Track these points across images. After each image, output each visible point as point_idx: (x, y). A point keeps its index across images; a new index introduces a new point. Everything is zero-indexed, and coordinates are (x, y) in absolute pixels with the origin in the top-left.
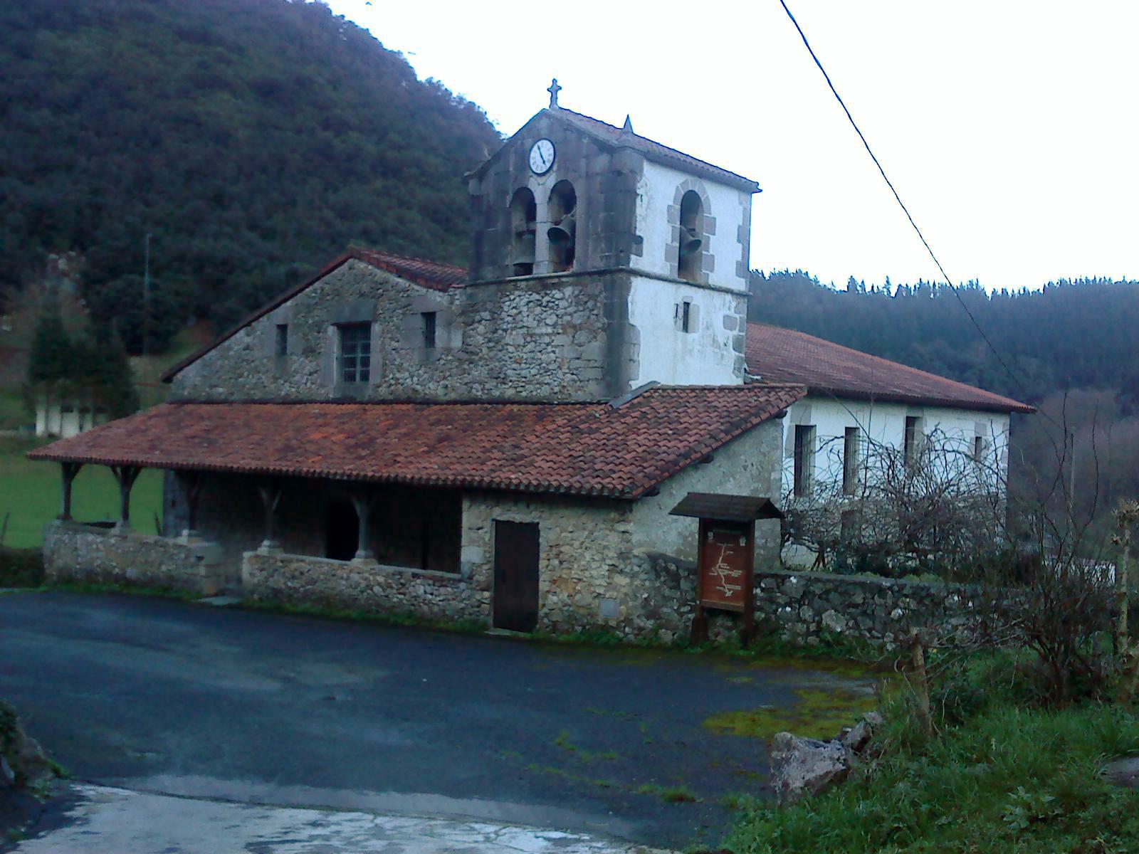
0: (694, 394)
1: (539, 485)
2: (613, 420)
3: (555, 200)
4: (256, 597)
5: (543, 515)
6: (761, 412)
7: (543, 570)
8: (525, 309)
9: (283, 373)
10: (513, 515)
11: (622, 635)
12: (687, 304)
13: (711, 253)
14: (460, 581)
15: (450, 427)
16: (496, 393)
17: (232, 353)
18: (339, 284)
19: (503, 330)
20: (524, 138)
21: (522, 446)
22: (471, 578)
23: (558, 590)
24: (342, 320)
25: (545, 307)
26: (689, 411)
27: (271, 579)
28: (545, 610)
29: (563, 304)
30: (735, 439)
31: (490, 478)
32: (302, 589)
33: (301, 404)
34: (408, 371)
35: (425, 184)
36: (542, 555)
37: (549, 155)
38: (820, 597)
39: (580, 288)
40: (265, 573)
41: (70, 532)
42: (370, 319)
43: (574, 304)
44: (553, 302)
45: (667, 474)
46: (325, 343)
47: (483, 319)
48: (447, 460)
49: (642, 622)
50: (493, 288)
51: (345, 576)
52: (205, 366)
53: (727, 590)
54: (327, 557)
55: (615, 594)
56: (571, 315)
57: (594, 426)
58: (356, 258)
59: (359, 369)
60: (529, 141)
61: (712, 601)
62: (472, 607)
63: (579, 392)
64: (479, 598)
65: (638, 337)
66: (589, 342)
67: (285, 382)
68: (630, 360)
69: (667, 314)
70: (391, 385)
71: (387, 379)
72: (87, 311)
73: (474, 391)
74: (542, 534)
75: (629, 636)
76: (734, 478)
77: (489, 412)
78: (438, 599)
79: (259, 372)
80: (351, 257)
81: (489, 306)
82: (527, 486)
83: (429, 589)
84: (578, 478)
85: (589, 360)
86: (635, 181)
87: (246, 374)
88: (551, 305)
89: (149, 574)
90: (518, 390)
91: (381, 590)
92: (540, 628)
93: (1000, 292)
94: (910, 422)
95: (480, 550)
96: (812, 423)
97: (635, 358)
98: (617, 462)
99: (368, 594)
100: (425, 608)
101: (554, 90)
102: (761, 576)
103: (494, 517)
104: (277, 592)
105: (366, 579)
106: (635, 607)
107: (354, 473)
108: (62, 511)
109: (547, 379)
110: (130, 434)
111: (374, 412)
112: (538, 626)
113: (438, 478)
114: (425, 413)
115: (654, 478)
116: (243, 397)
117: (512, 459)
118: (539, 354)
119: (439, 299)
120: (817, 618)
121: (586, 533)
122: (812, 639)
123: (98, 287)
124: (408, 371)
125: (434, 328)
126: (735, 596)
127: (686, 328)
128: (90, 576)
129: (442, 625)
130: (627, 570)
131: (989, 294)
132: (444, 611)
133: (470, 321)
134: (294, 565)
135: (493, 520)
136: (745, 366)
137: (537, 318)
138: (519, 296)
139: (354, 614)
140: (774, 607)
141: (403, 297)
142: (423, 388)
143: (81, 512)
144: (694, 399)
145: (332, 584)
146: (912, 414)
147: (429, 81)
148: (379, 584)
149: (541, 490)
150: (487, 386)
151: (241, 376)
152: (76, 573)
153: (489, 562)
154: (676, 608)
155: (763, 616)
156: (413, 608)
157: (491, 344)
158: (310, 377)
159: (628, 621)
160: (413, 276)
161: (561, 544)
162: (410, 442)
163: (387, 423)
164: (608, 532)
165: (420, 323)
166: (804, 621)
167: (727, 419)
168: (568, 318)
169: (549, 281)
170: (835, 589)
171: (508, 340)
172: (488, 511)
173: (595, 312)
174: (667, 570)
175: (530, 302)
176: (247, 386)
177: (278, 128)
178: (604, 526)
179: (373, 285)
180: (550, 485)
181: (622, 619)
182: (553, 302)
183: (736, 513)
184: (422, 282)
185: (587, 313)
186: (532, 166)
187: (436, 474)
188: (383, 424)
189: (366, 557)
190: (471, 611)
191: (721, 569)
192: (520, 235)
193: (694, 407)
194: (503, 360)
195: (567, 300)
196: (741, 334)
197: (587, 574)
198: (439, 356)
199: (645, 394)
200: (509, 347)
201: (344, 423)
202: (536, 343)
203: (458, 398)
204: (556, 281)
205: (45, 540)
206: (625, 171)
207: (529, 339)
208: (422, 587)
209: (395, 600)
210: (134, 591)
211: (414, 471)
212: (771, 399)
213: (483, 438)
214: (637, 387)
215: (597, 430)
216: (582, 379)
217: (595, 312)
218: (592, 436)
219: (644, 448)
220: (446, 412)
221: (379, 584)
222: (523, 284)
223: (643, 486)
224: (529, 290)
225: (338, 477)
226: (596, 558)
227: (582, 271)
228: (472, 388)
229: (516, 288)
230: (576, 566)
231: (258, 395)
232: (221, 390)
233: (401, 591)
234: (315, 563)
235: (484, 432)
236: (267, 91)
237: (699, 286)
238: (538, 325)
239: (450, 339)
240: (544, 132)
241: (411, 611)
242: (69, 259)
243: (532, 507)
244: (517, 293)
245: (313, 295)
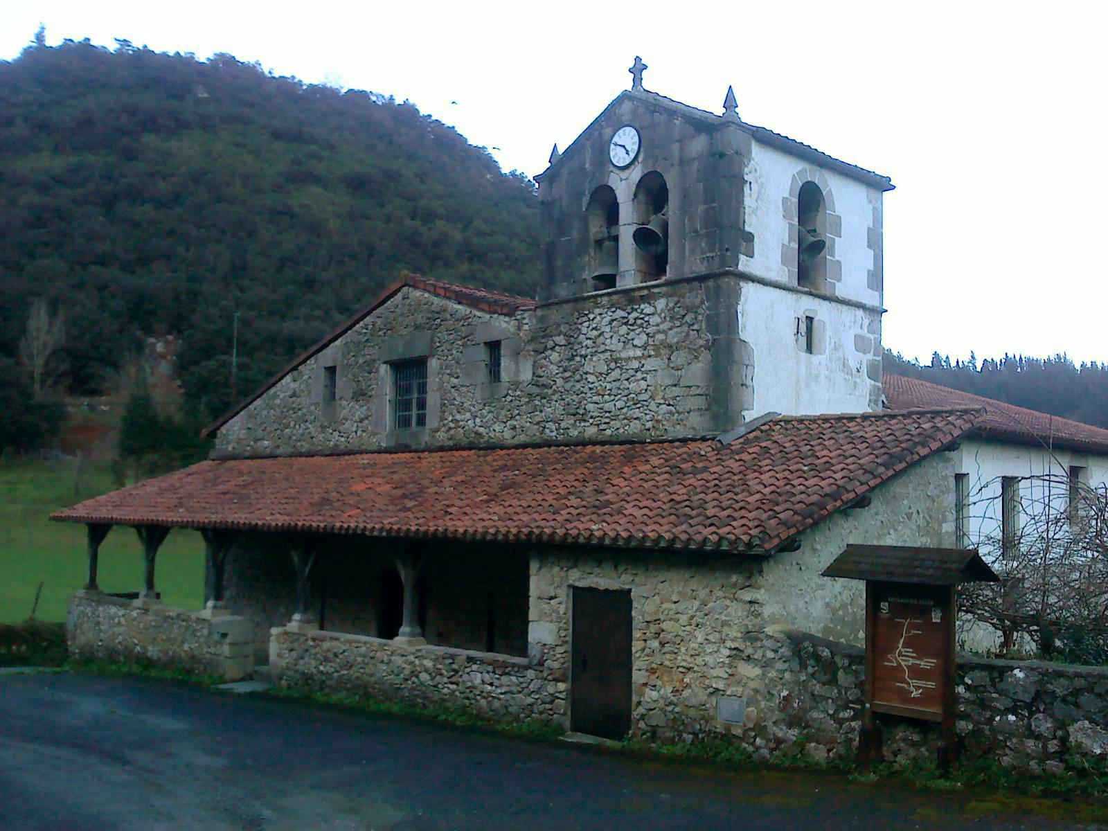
0: (829, 425)
1: (630, 537)
2: (724, 457)
3: (641, 197)
4: (284, 683)
5: (637, 580)
6: (929, 439)
7: (637, 655)
8: (608, 329)
9: (333, 422)
10: (596, 580)
11: (751, 749)
12: (810, 319)
13: (837, 258)
14: (527, 667)
15: (517, 472)
16: (574, 433)
17: (278, 401)
18: (392, 316)
19: (581, 356)
20: (602, 127)
21: (606, 491)
22: (541, 663)
23: (659, 683)
24: (395, 357)
25: (632, 325)
26: (826, 443)
27: (301, 662)
28: (641, 710)
29: (654, 320)
30: (898, 474)
31: (564, 531)
32: (336, 675)
33: (349, 455)
34: (470, 411)
35: (509, 267)
36: (636, 634)
37: (633, 144)
38: (1064, 700)
39: (676, 299)
40: (294, 654)
41: (93, 604)
42: (427, 354)
43: (668, 319)
44: (642, 319)
45: (809, 521)
46: (377, 384)
47: (556, 345)
48: (510, 510)
49: (781, 732)
50: (568, 307)
51: (386, 659)
52: (250, 417)
53: (912, 689)
54: (379, 637)
55: (740, 689)
56: (664, 332)
57: (700, 465)
58: (410, 286)
59: (414, 412)
60: (608, 131)
61: (895, 706)
62: (544, 703)
63: (678, 427)
64: (552, 692)
65: (751, 355)
66: (689, 364)
67: (335, 431)
68: (742, 385)
69: (786, 330)
70: (450, 428)
71: (446, 422)
72: (182, 390)
73: (547, 431)
74: (635, 604)
75: (762, 751)
76: (896, 530)
77: (565, 455)
78: (499, 691)
79: (306, 421)
80: (404, 286)
81: (563, 328)
82: (615, 539)
83: (487, 677)
84: (683, 527)
85: (690, 387)
86: (742, 165)
87: (292, 424)
88: (639, 322)
89: (171, 653)
90: (601, 428)
91: (428, 677)
92: (634, 735)
93: (1089, 365)
94: (1074, 472)
95: (553, 627)
96: (964, 471)
97: (749, 382)
98: (737, 506)
99: (414, 683)
100: (483, 702)
101: (638, 69)
102: (967, 667)
103: (571, 582)
104: (307, 677)
105: (411, 663)
106: (771, 710)
107: (395, 527)
108: (87, 579)
109: (637, 413)
110: (162, 491)
111: (430, 460)
112: (631, 732)
113: (498, 532)
114: (489, 458)
115: (794, 525)
116: (290, 450)
117: (595, 507)
118: (626, 382)
119: (504, 325)
120: (1059, 733)
121: (697, 603)
122: (1053, 765)
123: (192, 368)
124: (470, 411)
125: (499, 359)
126: (926, 697)
127: (809, 349)
128: (112, 655)
129: (503, 726)
130: (758, 655)
131: (1078, 367)
132: (506, 707)
133: (541, 347)
134: (327, 645)
135: (570, 586)
136: (883, 398)
137: (623, 339)
138: (600, 314)
139: (396, 709)
140: (988, 714)
141: (463, 325)
142: (487, 430)
143: (106, 582)
144: (830, 430)
145: (370, 669)
146: (1076, 464)
147: (513, 174)
148: (426, 670)
149: (633, 544)
150: (563, 425)
151: (287, 426)
152: (98, 651)
153: (566, 642)
154: (831, 712)
155: (971, 727)
156: (467, 702)
157: (567, 374)
158: (360, 424)
159: (760, 729)
160: (474, 302)
161: (662, 619)
162: (466, 491)
163: (443, 471)
164: (728, 602)
165: (483, 354)
166: (1038, 737)
167: (883, 451)
168: (661, 336)
169: (637, 294)
170: (1090, 690)
171: (588, 367)
172: (563, 574)
173: (696, 327)
174: (817, 657)
175: (613, 320)
176: (294, 438)
177: (367, 218)
178: (720, 594)
179: (430, 315)
180: (645, 537)
181: (751, 725)
182: (642, 319)
183: (930, 572)
184: (486, 307)
185: (686, 328)
186: (612, 159)
187: (495, 526)
188: (437, 472)
189: (412, 635)
190: (541, 708)
191: (902, 657)
192: (599, 243)
193: (832, 438)
194: (582, 393)
195: (660, 315)
196: (875, 358)
197: (699, 660)
198: (505, 393)
199: (763, 428)
200: (588, 376)
201: (394, 472)
202: (621, 369)
203: (528, 441)
204: (646, 292)
205: (69, 613)
206: (730, 152)
207: (613, 365)
208: (479, 675)
209: (445, 691)
210: (153, 673)
211: (468, 523)
212: (939, 425)
213: (557, 483)
214: (752, 419)
215: (705, 469)
216: (680, 410)
217: (696, 327)
218: (699, 477)
219: (773, 488)
220: (513, 456)
221: (426, 670)
222: (605, 299)
223: (778, 536)
224: (612, 306)
225: (376, 533)
226: (710, 637)
227: (678, 278)
228: (544, 428)
229: (597, 305)
230: (683, 650)
231: (305, 447)
232: (266, 443)
233: (453, 679)
234: (350, 642)
235: (559, 477)
236: (357, 184)
237: (824, 298)
238: (624, 348)
239: (517, 371)
240: (625, 119)
241: (465, 706)
242: (167, 343)
243: (621, 569)
244: (597, 311)
245: (364, 331)
